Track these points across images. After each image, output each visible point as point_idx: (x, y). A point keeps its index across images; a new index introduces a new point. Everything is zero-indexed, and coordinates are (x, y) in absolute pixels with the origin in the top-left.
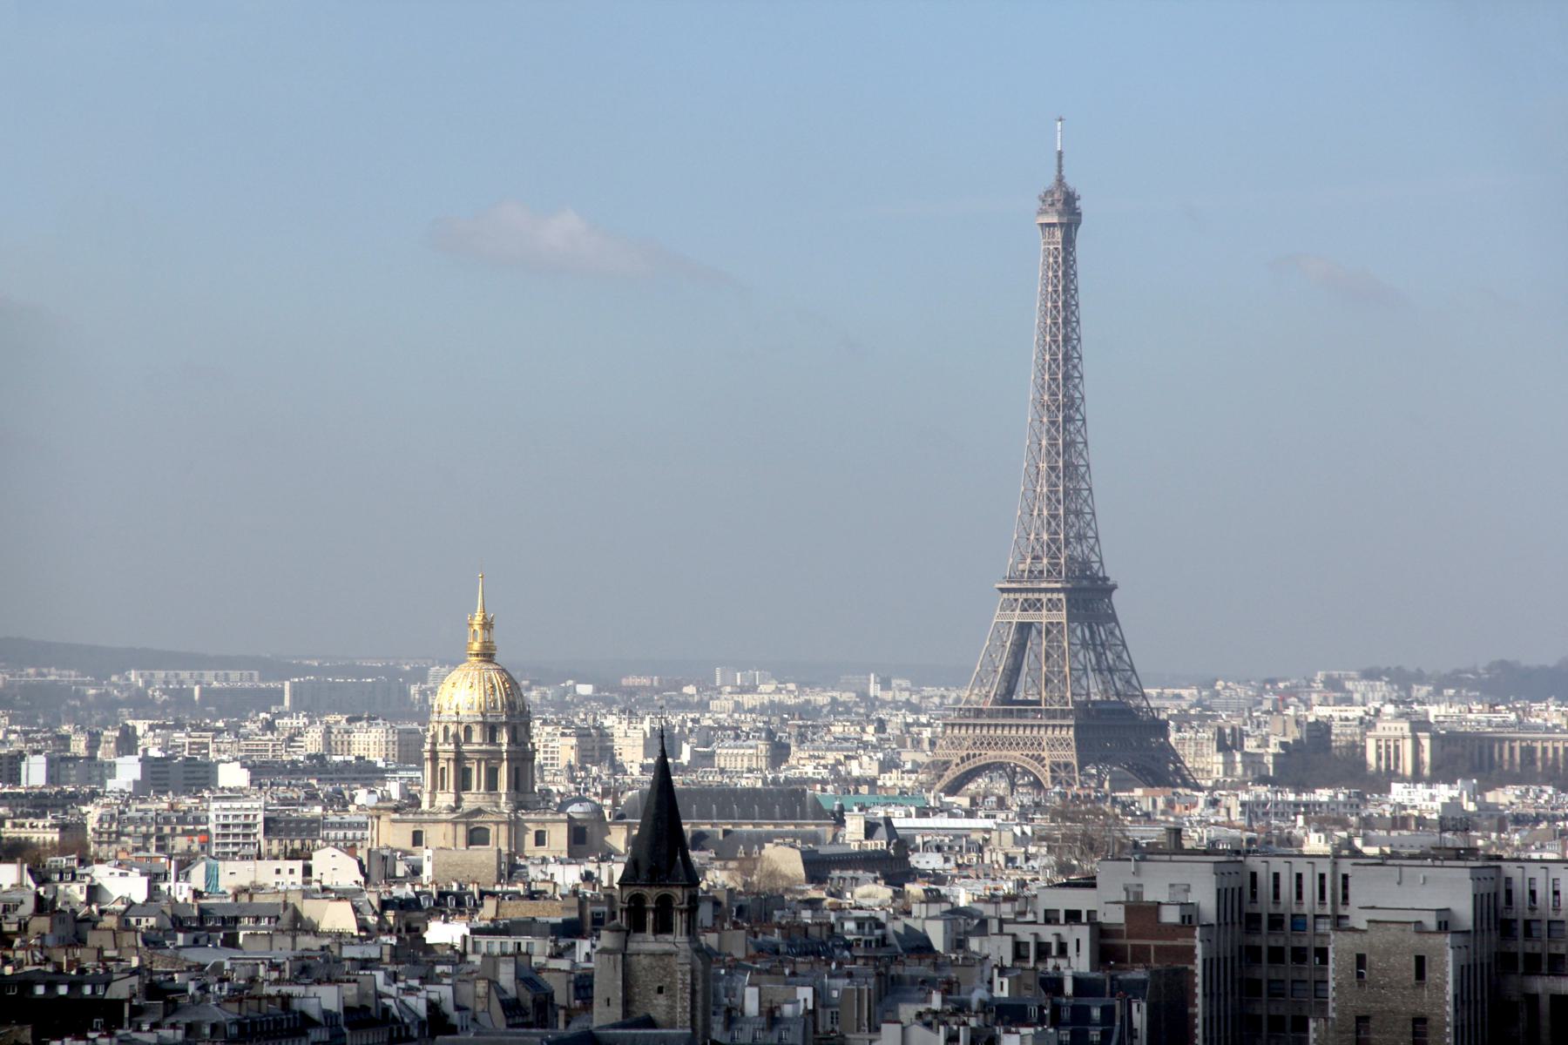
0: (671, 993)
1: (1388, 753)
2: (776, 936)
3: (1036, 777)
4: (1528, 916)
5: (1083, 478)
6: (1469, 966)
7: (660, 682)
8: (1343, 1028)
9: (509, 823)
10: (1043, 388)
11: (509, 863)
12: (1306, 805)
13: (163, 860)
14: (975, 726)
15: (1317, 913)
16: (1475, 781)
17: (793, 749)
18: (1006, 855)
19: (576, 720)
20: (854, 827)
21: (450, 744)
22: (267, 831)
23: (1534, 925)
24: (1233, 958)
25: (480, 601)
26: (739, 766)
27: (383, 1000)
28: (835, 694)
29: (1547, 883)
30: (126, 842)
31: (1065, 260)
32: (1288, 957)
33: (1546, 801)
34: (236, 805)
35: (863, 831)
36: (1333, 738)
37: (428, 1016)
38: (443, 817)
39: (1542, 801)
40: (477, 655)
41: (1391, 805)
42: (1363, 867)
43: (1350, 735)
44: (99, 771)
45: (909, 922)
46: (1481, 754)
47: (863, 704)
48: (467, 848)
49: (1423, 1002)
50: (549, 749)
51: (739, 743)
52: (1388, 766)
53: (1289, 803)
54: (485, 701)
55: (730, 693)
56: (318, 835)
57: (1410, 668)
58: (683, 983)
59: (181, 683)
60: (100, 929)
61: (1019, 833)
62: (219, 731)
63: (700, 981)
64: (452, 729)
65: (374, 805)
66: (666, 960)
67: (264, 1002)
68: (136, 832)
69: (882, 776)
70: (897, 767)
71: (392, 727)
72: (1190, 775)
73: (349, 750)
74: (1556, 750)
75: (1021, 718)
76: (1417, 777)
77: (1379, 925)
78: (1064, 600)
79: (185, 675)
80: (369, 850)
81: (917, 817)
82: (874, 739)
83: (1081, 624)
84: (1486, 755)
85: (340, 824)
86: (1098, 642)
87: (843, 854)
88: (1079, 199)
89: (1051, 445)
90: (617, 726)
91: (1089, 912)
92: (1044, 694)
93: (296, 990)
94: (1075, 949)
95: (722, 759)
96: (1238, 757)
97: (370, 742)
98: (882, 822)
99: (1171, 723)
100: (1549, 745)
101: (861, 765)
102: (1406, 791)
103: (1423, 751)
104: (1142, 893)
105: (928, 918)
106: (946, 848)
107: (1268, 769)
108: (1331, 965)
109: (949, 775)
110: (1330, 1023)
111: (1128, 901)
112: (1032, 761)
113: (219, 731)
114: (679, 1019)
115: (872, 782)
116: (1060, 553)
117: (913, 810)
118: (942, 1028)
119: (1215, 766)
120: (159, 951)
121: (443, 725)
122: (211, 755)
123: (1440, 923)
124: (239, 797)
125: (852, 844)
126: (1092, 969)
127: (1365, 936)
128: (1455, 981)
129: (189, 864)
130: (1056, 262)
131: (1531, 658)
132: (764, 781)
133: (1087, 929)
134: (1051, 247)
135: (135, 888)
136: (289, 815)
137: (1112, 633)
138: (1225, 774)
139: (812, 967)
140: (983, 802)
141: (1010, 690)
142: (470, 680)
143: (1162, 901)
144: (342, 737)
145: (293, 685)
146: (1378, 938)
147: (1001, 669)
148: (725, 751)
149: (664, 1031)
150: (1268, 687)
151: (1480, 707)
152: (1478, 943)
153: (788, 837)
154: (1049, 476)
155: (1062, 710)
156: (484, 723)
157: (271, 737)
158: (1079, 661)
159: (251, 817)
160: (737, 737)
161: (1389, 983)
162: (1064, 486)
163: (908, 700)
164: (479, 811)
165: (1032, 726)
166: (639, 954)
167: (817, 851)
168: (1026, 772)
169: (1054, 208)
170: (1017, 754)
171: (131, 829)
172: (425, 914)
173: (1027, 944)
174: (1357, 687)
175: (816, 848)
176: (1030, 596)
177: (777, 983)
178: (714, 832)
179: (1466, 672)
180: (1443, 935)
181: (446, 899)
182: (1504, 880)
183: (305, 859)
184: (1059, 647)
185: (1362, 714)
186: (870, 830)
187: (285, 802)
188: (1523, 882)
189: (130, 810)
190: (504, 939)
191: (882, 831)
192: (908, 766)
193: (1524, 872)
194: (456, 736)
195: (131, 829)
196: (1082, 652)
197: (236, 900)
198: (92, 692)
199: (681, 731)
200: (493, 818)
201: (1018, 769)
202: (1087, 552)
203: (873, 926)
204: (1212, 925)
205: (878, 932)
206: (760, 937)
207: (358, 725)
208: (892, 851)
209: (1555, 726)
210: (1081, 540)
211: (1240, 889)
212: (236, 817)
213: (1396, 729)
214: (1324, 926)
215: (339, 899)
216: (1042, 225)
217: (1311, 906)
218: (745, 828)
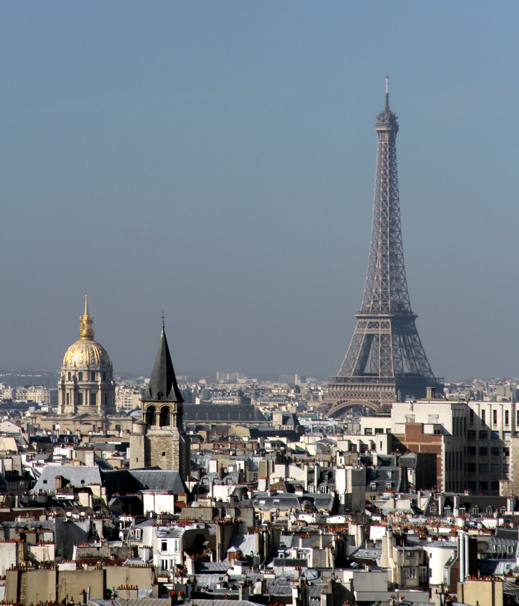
0: (169, 455)
5: (400, 261)
10: (379, 215)
15: (504, 430)
24: (461, 452)
25: (86, 307)
27: (26, 469)
31: (390, 150)
35: (281, 420)
38: (69, 418)
40: (85, 336)
50: (128, 401)
51: (225, 397)
54: (89, 360)
55: (223, 383)
58: (175, 450)
63: (184, 449)
64: (72, 374)
65: (33, 412)
75: (368, 382)
78: (390, 323)
80: (28, 425)
82: (294, 396)
83: (399, 335)
88: (397, 118)
89: (383, 244)
91: (387, 429)
92: (380, 370)
98: (291, 416)
104: (414, 419)
105: (308, 444)
106: (325, 431)
108: (511, 455)
111: (407, 423)
112: (376, 405)
118: (306, 467)
121: (68, 371)
125: (276, 427)
126: (389, 453)
133: (386, 436)
134: (383, 143)
137: (415, 340)
139: (245, 452)
141: (362, 368)
142: (81, 349)
144: (22, 394)
147: (357, 358)
154: (382, 259)
155: (389, 378)
156: (89, 371)
158: (398, 354)
160: (224, 395)
162: (390, 265)
164: (86, 415)
170: (366, 400)
176: (373, 320)
177: (226, 459)
178: (207, 426)
181: (64, 439)
184: (388, 346)
186: (285, 420)
194: (75, 377)
200: (94, 419)
201: (367, 409)
202: (401, 299)
203: (280, 445)
205: (282, 448)
208: (297, 431)
210: (399, 292)
215: (8, 436)
216: (378, 131)
217: (501, 426)
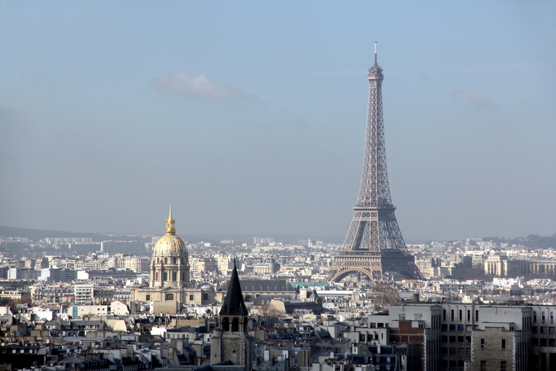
0: (238, 352)
1: (492, 267)
2: (275, 332)
3: (367, 276)
4: (542, 325)
5: (384, 170)
6: (521, 343)
7: (234, 242)
8: (476, 365)
9: (181, 292)
10: (370, 138)
11: (181, 306)
12: (463, 286)
13: (58, 305)
14: (346, 258)
15: (467, 324)
16: (523, 277)
17: (281, 266)
18: (357, 304)
19: (204, 256)
20: (303, 294)
21: (159, 264)
22: (95, 295)
23: (544, 329)
24: (437, 340)
25: (170, 213)
26: (262, 272)
27: (136, 355)
28: (296, 246)
29: (549, 314)
30: (45, 299)
31: (378, 92)
32: (457, 340)
33: (548, 284)
34: (84, 286)
35: (306, 295)
36: (473, 262)
37: (152, 361)
38: (157, 290)
39: (547, 284)
40: (169, 233)
41: (493, 286)
42: (483, 308)
43: (479, 261)
44: (35, 274)
45: (322, 327)
46: (525, 268)
47: (306, 250)
48: (166, 301)
49: (505, 356)
50: (195, 266)
51: (262, 264)
52: (492, 272)
53: (457, 285)
54: (172, 249)
55: (259, 246)
56: (113, 296)
57: (500, 237)
58: (242, 349)
59: (64, 242)
60: (36, 330)
61: (361, 296)
62: (78, 260)
63: (248, 348)
64: (160, 259)
65: (132, 286)
66: (236, 341)
67: (94, 356)
68: (48, 295)
69: (313, 275)
70: (318, 272)
71: (139, 258)
72: (422, 275)
73: (124, 266)
74: (552, 266)
75: (362, 255)
76: (502, 276)
77: (489, 329)
78: (377, 213)
79: (65, 239)
80: (131, 302)
81: (325, 290)
82: (310, 262)
83: (383, 221)
84: (527, 268)
85: (121, 292)
86: (389, 228)
87: (299, 303)
88: (383, 71)
89: (373, 158)
90: (219, 258)
91: (386, 324)
92: (370, 246)
93: (105, 351)
94: (381, 337)
95: (256, 269)
96: (439, 269)
97: (131, 264)
98: (313, 292)
99: (415, 257)
100: (549, 264)
101: (305, 272)
102: (498, 281)
103: (504, 267)
104: (405, 317)
105: (329, 326)
106: (335, 301)
107: (450, 273)
108: (472, 343)
109: (337, 275)
110: (472, 363)
111: (400, 320)
112: (367, 271)
113: (78, 260)
114: (241, 362)
115: (309, 278)
116: (376, 196)
117: (324, 287)
118: (334, 365)
119: (431, 272)
120: (56, 338)
121: (157, 257)
122: (75, 268)
123: (510, 328)
124: (85, 283)
125: (302, 300)
126: (387, 344)
127: (484, 332)
128: (516, 348)
129: (67, 307)
130: (374, 93)
131: (543, 234)
132: (271, 277)
133: (385, 330)
134: (373, 88)
135: (48, 315)
136: (102, 289)
137: (394, 225)
138: (435, 275)
139: (288, 343)
140: (349, 285)
141: (358, 245)
142: (166, 241)
143: (412, 320)
144: (121, 262)
145: (104, 243)
146: (489, 333)
147: (355, 237)
148: (257, 267)
149: (235, 366)
150: (450, 244)
151: (525, 251)
152: (524, 335)
153: (279, 297)
154: (372, 169)
155: (377, 252)
156: (171, 257)
157: (96, 262)
158: (383, 235)
159: (89, 290)
160: (261, 262)
161: (493, 349)
162: (377, 173)
163: (322, 248)
164: (170, 288)
165: (366, 258)
166: (226, 339)
167: (290, 302)
168: (364, 274)
169: (374, 74)
170: (361, 268)
171: (46, 294)
172: (151, 324)
173: (364, 335)
174: (481, 244)
175: (289, 301)
176: (365, 211)
177: (276, 349)
178: (253, 295)
179: (520, 239)
180: (512, 332)
181: (158, 319)
182: (533, 312)
183: (108, 305)
184: (376, 230)
185: (483, 253)
186: (309, 295)
187: (101, 285)
188: (540, 313)
189: (46, 288)
190: (179, 333)
191: (313, 295)
192: (322, 272)
193: (540, 310)
194: (162, 261)
195: (46, 294)
196: (384, 231)
197: (84, 319)
198: (33, 246)
199: (242, 260)
200: (175, 291)
201: (361, 273)
202: (385, 196)
203: (310, 329)
204: (430, 328)
205: (311, 331)
206: (270, 333)
207: (127, 257)
208: (316, 302)
209: (552, 258)
210: (383, 192)
211: (440, 316)
212: (84, 290)
213: (495, 259)
214: (470, 329)
215: (120, 319)
216: (369, 80)
217: (465, 322)
218: (264, 294)
